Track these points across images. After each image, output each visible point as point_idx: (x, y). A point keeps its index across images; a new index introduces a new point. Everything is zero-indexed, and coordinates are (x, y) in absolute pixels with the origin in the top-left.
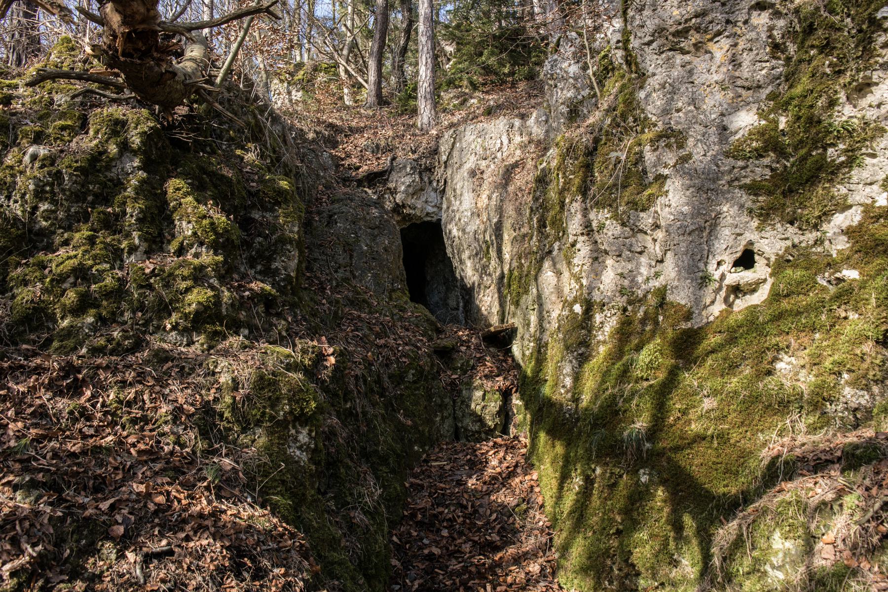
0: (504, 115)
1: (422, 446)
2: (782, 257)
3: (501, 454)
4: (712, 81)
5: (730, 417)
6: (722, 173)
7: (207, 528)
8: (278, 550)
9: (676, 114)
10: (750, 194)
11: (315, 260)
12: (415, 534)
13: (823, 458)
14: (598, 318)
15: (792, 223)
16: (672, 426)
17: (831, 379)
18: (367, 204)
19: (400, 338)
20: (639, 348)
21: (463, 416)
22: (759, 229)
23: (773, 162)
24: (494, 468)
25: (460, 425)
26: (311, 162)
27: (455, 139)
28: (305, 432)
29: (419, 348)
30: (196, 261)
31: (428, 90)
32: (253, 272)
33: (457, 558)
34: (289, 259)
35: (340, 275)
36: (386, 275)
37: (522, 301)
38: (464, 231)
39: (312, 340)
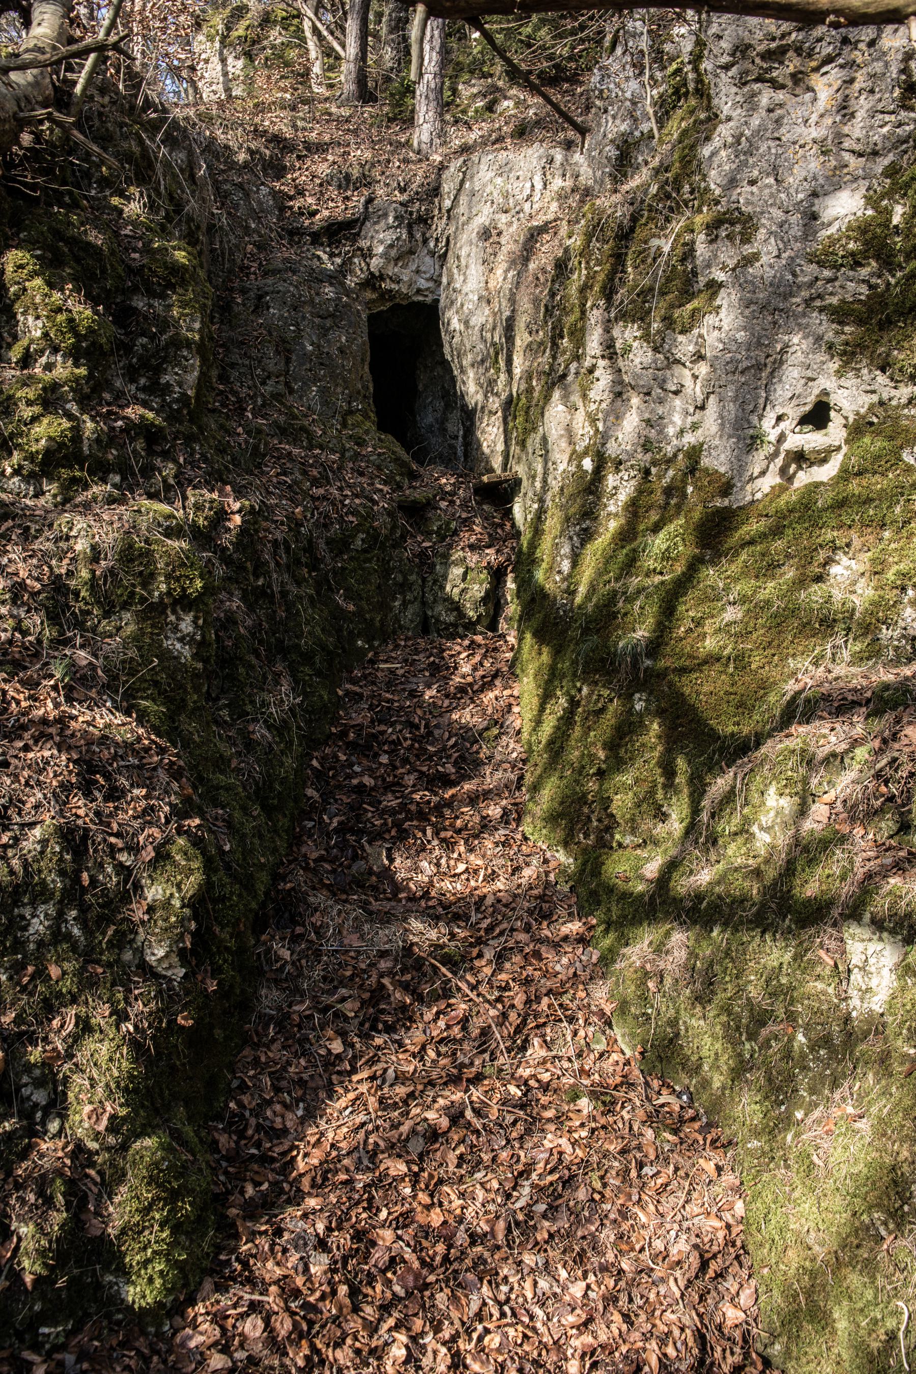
0: (542, 141)
1: (369, 641)
2: (864, 417)
3: (477, 658)
4: (808, 139)
5: (755, 636)
6: (799, 287)
7: (50, 737)
8: (141, 767)
9: (748, 189)
10: (833, 322)
11: (233, 365)
12: (343, 758)
13: (850, 698)
14: (611, 480)
15: (883, 370)
16: (681, 639)
17: (892, 595)
18: (318, 277)
19: (349, 486)
20: (656, 529)
21: (435, 601)
22: (839, 374)
23: (872, 275)
24: (464, 677)
25: (430, 613)
26: (236, 207)
27: (464, 173)
28: (188, 618)
29: (375, 503)
30: (48, 377)
31: (433, 86)
32: (133, 387)
33: (394, 792)
34: (185, 369)
35: (268, 389)
36: (339, 390)
37: (529, 442)
38: (466, 323)
39: (212, 491)
